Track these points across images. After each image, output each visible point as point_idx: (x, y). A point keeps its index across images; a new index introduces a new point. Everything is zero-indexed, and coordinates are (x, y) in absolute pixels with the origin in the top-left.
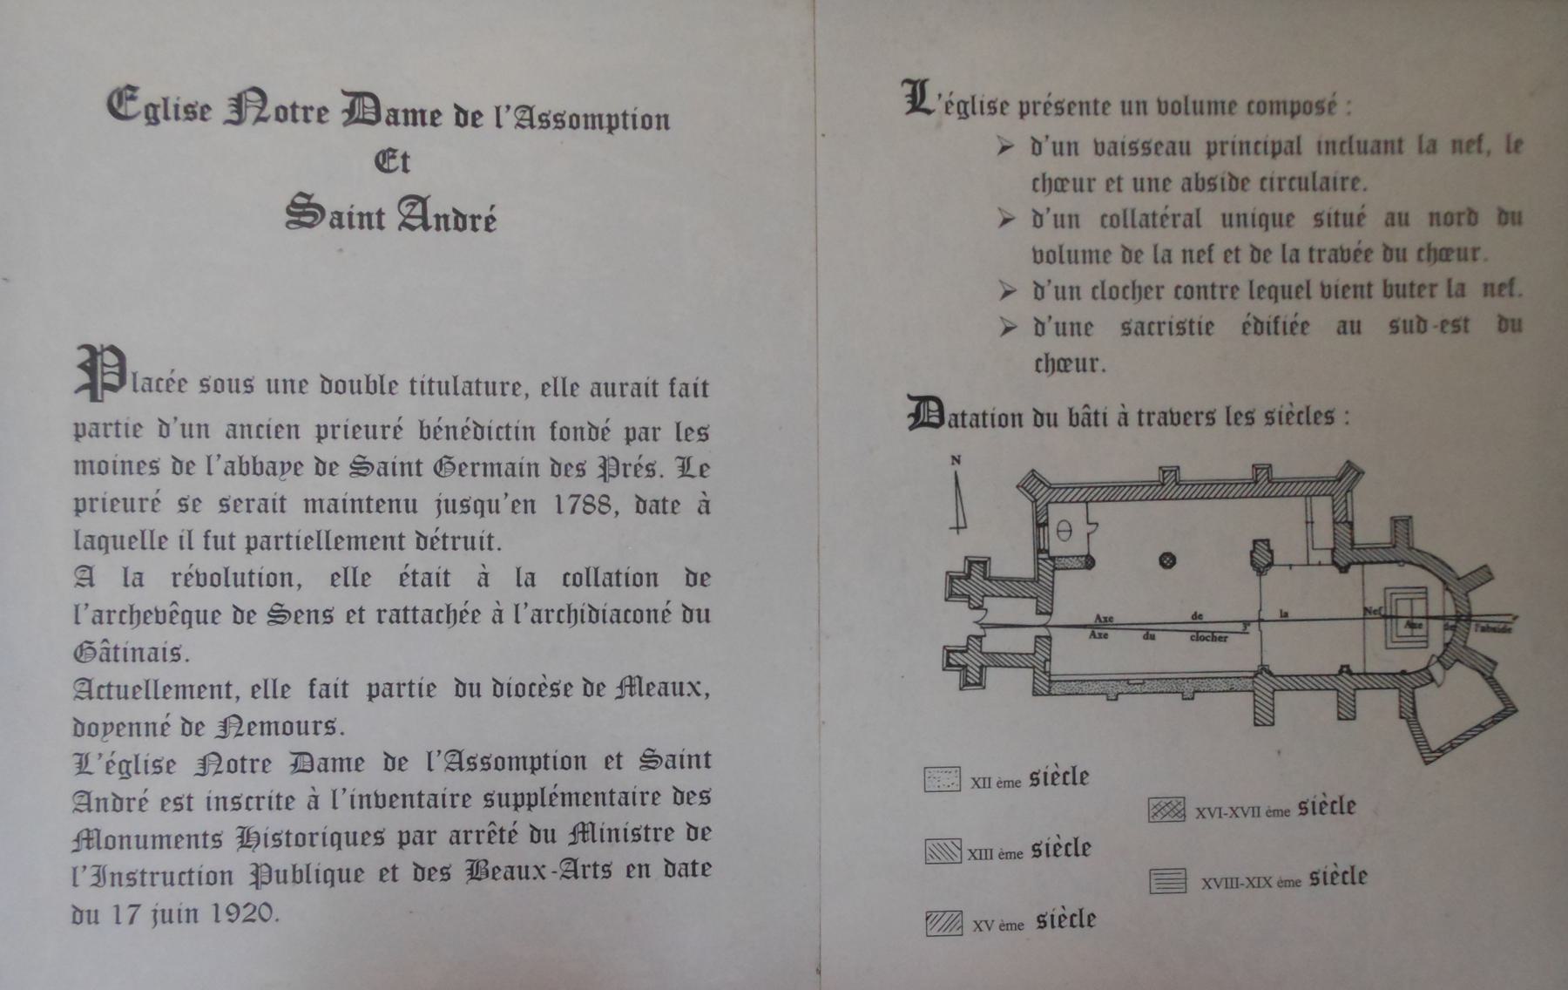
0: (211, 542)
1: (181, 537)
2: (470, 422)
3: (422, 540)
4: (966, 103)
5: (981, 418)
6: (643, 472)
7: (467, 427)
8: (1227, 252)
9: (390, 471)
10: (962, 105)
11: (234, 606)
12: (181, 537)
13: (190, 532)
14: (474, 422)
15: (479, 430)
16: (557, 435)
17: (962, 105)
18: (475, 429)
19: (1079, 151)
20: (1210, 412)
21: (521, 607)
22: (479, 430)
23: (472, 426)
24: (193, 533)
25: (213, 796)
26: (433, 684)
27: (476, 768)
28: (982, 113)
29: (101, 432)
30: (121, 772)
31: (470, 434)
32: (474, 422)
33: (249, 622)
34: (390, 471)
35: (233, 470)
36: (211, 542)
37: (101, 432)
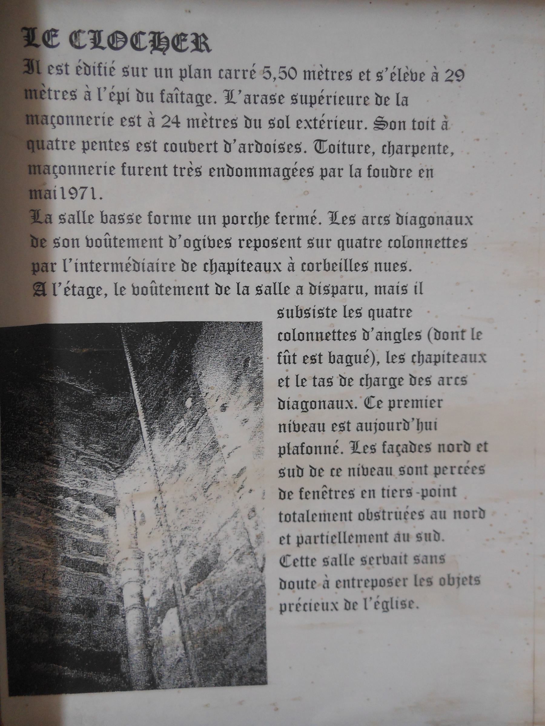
0: (126, 170)
1: (416, 287)
2: (131, 259)
3: (282, 494)
4: (387, 602)
5: (363, 242)
6: (193, 173)
7: (129, 263)
8: (479, 446)
9: (174, 100)
10: (385, 604)
11: (216, 284)
12: (416, 287)
13: (421, 283)
14: (134, 260)
15: (137, 265)
16: (152, 220)
17: (385, 604)
18: (134, 265)
19: (375, 495)
20: (386, 217)
21: (102, 90)
22: (137, 265)
23: (132, 263)
24: (422, 284)
25: (160, 262)
26: (113, 167)
27: (124, 222)
28: (397, 608)
29: (233, 75)
30: (383, 608)
31: (131, 268)
32: (134, 260)
33: (192, 270)
34: (174, 100)
35: (249, 101)
36: (126, 170)
37: (233, 75)
